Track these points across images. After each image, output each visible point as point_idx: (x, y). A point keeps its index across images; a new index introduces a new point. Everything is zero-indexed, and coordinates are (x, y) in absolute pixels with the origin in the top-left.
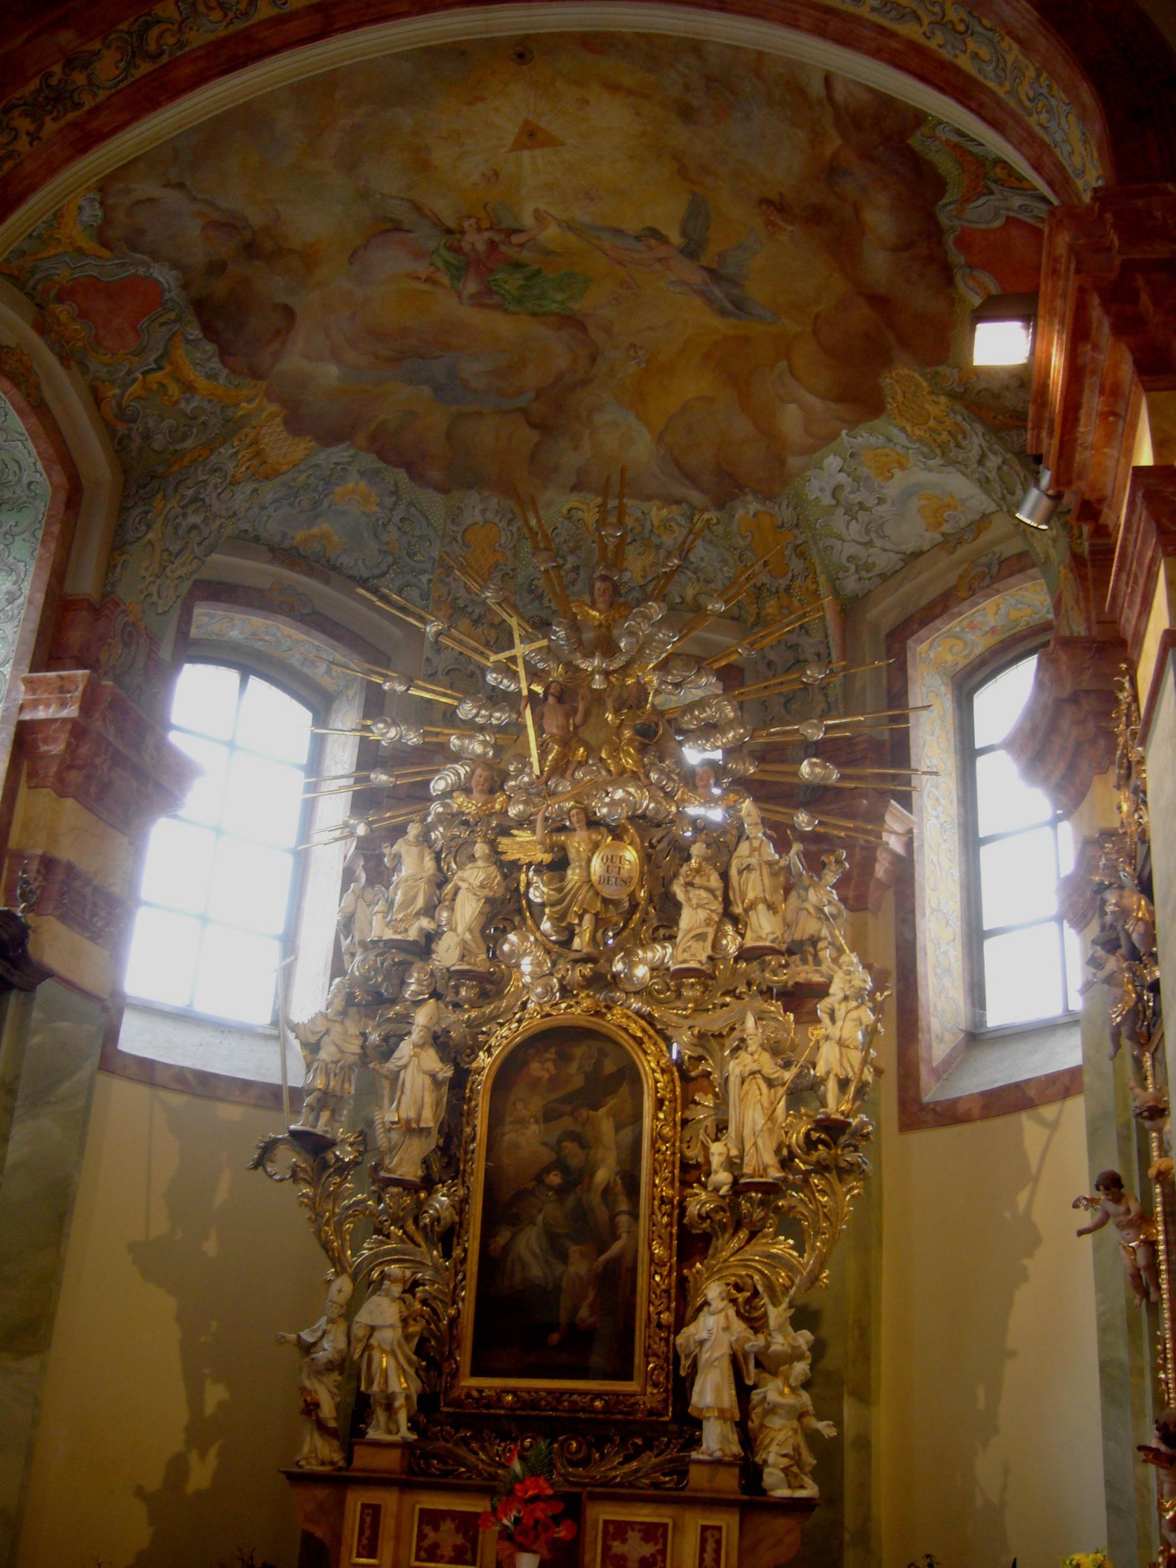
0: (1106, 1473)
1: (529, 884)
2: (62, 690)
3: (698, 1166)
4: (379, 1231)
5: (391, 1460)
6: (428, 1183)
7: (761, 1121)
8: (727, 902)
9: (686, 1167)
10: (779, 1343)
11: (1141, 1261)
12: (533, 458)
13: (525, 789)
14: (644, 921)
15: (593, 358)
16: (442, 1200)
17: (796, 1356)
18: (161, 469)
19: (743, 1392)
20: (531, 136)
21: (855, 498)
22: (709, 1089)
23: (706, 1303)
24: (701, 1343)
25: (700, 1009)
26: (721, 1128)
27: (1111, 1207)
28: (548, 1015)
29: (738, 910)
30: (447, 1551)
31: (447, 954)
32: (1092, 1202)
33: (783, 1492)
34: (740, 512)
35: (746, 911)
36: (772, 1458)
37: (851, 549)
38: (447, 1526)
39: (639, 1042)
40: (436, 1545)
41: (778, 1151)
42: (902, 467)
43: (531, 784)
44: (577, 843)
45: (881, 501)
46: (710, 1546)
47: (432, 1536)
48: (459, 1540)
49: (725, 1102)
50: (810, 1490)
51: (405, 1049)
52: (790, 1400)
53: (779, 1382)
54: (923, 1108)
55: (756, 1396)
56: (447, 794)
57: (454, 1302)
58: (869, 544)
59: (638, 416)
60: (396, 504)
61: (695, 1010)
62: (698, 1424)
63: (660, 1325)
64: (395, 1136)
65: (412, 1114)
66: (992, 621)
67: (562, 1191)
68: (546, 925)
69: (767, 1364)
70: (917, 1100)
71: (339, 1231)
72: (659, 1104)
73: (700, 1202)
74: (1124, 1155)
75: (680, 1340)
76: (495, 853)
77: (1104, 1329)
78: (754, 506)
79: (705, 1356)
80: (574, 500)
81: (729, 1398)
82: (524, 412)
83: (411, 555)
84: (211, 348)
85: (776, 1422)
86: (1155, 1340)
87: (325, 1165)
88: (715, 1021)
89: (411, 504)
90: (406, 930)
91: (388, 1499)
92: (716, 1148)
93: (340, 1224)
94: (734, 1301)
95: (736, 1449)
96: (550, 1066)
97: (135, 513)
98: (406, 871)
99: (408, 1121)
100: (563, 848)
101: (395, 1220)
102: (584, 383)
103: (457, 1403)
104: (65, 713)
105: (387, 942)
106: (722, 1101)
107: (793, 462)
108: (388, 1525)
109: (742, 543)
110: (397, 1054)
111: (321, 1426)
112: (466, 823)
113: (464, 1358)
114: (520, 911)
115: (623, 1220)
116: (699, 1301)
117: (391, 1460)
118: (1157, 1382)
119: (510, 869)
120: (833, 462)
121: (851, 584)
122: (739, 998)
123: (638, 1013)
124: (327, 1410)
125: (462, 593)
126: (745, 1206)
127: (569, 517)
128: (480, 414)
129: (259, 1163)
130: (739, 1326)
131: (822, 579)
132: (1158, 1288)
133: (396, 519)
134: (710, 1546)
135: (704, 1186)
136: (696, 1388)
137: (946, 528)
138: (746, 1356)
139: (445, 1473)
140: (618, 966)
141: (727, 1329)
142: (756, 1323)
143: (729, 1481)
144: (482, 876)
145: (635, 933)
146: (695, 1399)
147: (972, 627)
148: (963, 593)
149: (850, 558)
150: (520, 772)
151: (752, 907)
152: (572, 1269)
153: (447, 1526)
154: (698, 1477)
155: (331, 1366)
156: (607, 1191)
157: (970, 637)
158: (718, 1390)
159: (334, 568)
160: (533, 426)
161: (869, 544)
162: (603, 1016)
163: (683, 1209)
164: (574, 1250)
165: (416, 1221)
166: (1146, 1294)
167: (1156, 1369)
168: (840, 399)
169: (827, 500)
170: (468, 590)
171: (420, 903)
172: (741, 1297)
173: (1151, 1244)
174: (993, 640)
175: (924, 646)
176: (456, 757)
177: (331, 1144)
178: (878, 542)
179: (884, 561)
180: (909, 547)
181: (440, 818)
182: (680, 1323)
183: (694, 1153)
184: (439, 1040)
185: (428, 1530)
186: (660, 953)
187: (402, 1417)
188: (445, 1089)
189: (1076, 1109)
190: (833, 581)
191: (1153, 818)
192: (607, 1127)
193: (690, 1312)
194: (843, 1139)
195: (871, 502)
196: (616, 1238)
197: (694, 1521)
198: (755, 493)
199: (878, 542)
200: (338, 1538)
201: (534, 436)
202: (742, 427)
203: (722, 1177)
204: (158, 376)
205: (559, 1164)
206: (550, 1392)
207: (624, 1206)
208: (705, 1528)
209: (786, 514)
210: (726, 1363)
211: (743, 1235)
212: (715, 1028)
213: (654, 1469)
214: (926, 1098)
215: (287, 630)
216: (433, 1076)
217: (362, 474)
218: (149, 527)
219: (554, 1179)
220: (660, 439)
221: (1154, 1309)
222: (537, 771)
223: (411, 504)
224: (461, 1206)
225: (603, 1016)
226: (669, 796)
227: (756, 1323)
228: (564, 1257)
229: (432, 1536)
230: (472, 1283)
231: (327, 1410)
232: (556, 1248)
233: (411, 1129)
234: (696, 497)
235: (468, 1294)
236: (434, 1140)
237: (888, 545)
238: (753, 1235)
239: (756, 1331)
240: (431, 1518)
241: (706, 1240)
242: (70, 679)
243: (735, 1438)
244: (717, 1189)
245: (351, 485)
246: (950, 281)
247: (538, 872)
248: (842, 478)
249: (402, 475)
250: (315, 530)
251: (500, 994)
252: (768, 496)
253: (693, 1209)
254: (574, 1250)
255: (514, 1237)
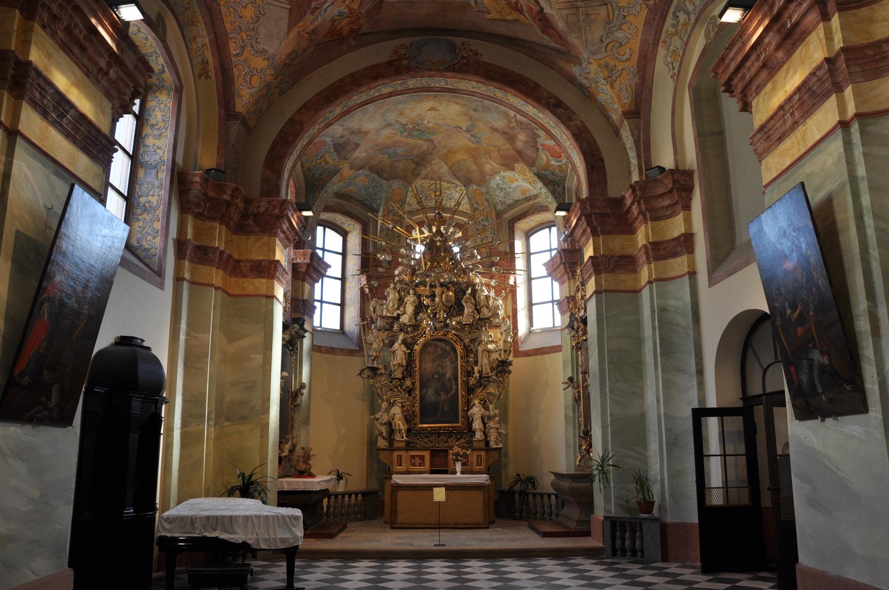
0: (566, 438)
1: (424, 300)
2: (304, 255)
3: (470, 372)
4: (391, 390)
5: (403, 445)
6: (404, 378)
7: (487, 362)
8: (476, 306)
9: (468, 372)
10: (492, 413)
11: (577, 395)
12: (413, 171)
13: (421, 274)
14: (454, 310)
15: (434, 148)
16: (408, 383)
17: (495, 416)
18: (316, 183)
19: (485, 424)
20: (432, 109)
21: (503, 186)
22: (472, 353)
23: (474, 404)
24: (474, 414)
25: (469, 333)
26: (476, 363)
27: (571, 384)
28: (432, 336)
29: (478, 308)
30: (418, 464)
31: (405, 319)
32: (566, 383)
33: (495, 446)
34: (471, 188)
35: (480, 308)
36: (492, 439)
37: (500, 199)
38: (417, 458)
39: (456, 342)
40: (415, 463)
41: (491, 368)
42: (517, 181)
43: (423, 273)
44: (438, 291)
45: (510, 188)
46: (479, 459)
47: (414, 461)
48: (420, 461)
49: (477, 356)
50: (501, 446)
51: (396, 345)
52: (495, 426)
53: (492, 422)
54: (519, 352)
55: (487, 425)
56: (398, 275)
57: (413, 407)
58: (505, 197)
59: (444, 162)
60: (373, 183)
61: (468, 333)
62: (474, 432)
63: (464, 410)
64: (396, 367)
65: (400, 362)
66: (537, 219)
67: (438, 380)
68: (429, 311)
69: (490, 418)
70: (518, 350)
71: (381, 391)
72: (462, 357)
73: (472, 381)
74: (573, 372)
75: (469, 413)
76: (415, 294)
77: (566, 408)
78: (475, 187)
79: (475, 417)
80: (423, 181)
81: (482, 426)
82: (413, 160)
83: (375, 195)
84: (335, 153)
85: (492, 431)
86: (578, 412)
87: (376, 374)
88: (473, 336)
89: (377, 183)
90: (393, 314)
91: (403, 453)
92: (476, 368)
93: (381, 389)
94: (480, 404)
95: (484, 438)
96: (433, 348)
97: (311, 196)
98: (391, 297)
99: (399, 364)
100: (434, 292)
101: (396, 388)
102: (430, 154)
103: (417, 430)
104: (306, 261)
105: (388, 317)
106: (476, 356)
107: (487, 178)
108: (403, 459)
109: (471, 196)
110: (394, 346)
111: (383, 437)
112: (406, 284)
113: (417, 420)
114: (421, 307)
115: (454, 386)
116: (472, 404)
117: (403, 445)
118: (579, 420)
119: (419, 296)
120: (498, 178)
121: (499, 207)
122: (479, 330)
123: (454, 334)
124: (385, 434)
125: (391, 208)
126: (483, 382)
127: (421, 186)
128: (400, 160)
129: (360, 374)
130: (483, 410)
131: (493, 207)
132: (580, 401)
133: (372, 186)
134: (479, 459)
135: (473, 377)
136: (474, 425)
137: (526, 195)
138: (485, 416)
139: (414, 447)
140: (448, 322)
141: (480, 411)
142: (487, 409)
143: (483, 445)
144: (413, 299)
145: (452, 313)
146: (473, 427)
147: (532, 221)
148: (530, 213)
149: (500, 201)
150: (419, 269)
151: (482, 307)
152: (442, 398)
153: (417, 458)
154: (475, 445)
155: (385, 424)
156: (449, 380)
157: (531, 223)
158: (479, 425)
159: (352, 198)
160: (414, 163)
161: (505, 197)
162: (446, 336)
163: (468, 383)
164: (442, 393)
165: (401, 387)
166: (577, 402)
167: (579, 418)
168: (503, 165)
169: (495, 187)
170: (392, 206)
171: (396, 306)
172: (482, 403)
173: (579, 392)
174: (537, 223)
175: (518, 225)
176: (401, 264)
177: (377, 369)
178: (508, 197)
179: (509, 201)
180: (516, 199)
181: (398, 281)
182: (468, 410)
183: (469, 369)
184: (404, 342)
185: (412, 459)
186: (458, 318)
187: (404, 435)
188: (407, 355)
189: (559, 356)
190: (495, 206)
191: (588, 315)
192: (448, 363)
193: (470, 407)
194: (506, 365)
195: (507, 188)
196: (452, 390)
197: (476, 454)
198: (476, 184)
199: (508, 197)
200: (392, 463)
201: (414, 166)
202: (474, 168)
203: (477, 375)
204: (320, 160)
205: (438, 373)
206: (439, 427)
207: (454, 382)
208: (478, 455)
209: (484, 190)
210: (480, 418)
211: (482, 388)
212: (473, 338)
213: (463, 443)
214: (520, 350)
215: (338, 216)
216: (405, 352)
217: (365, 175)
218: (316, 201)
219: (436, 376)
220: (450, 168)
221: (579, 406)
222: (424, 268)
223: (377, 183)
224: (413, 384)
225: (446, 336)
226: (460, 276)
227: (487, 409)
228: (440, 395)
229: (414, 461)
230: (418, 402)
231: (385, 434)
232: (437, 393)
233: (400, 365)
234: (458, 183)
235: (417, 405)
236: (405, 367)
237: (510, 198)
238: (484, 388)
239: (486, 410)
240: (413, 457)
241: (473, 389)
242: (306, 252)
243: (483, 435)
244: (476, 378)
245: (361, 178)
246: (538, 151)
247: (426, 297)
248: (500, 182)
249: (376, 175)
250: (349, 189)
251: (418, 329)
252: (479, 185)
253: (471, 383)
254: (442, 393)
255: (427, 390)
